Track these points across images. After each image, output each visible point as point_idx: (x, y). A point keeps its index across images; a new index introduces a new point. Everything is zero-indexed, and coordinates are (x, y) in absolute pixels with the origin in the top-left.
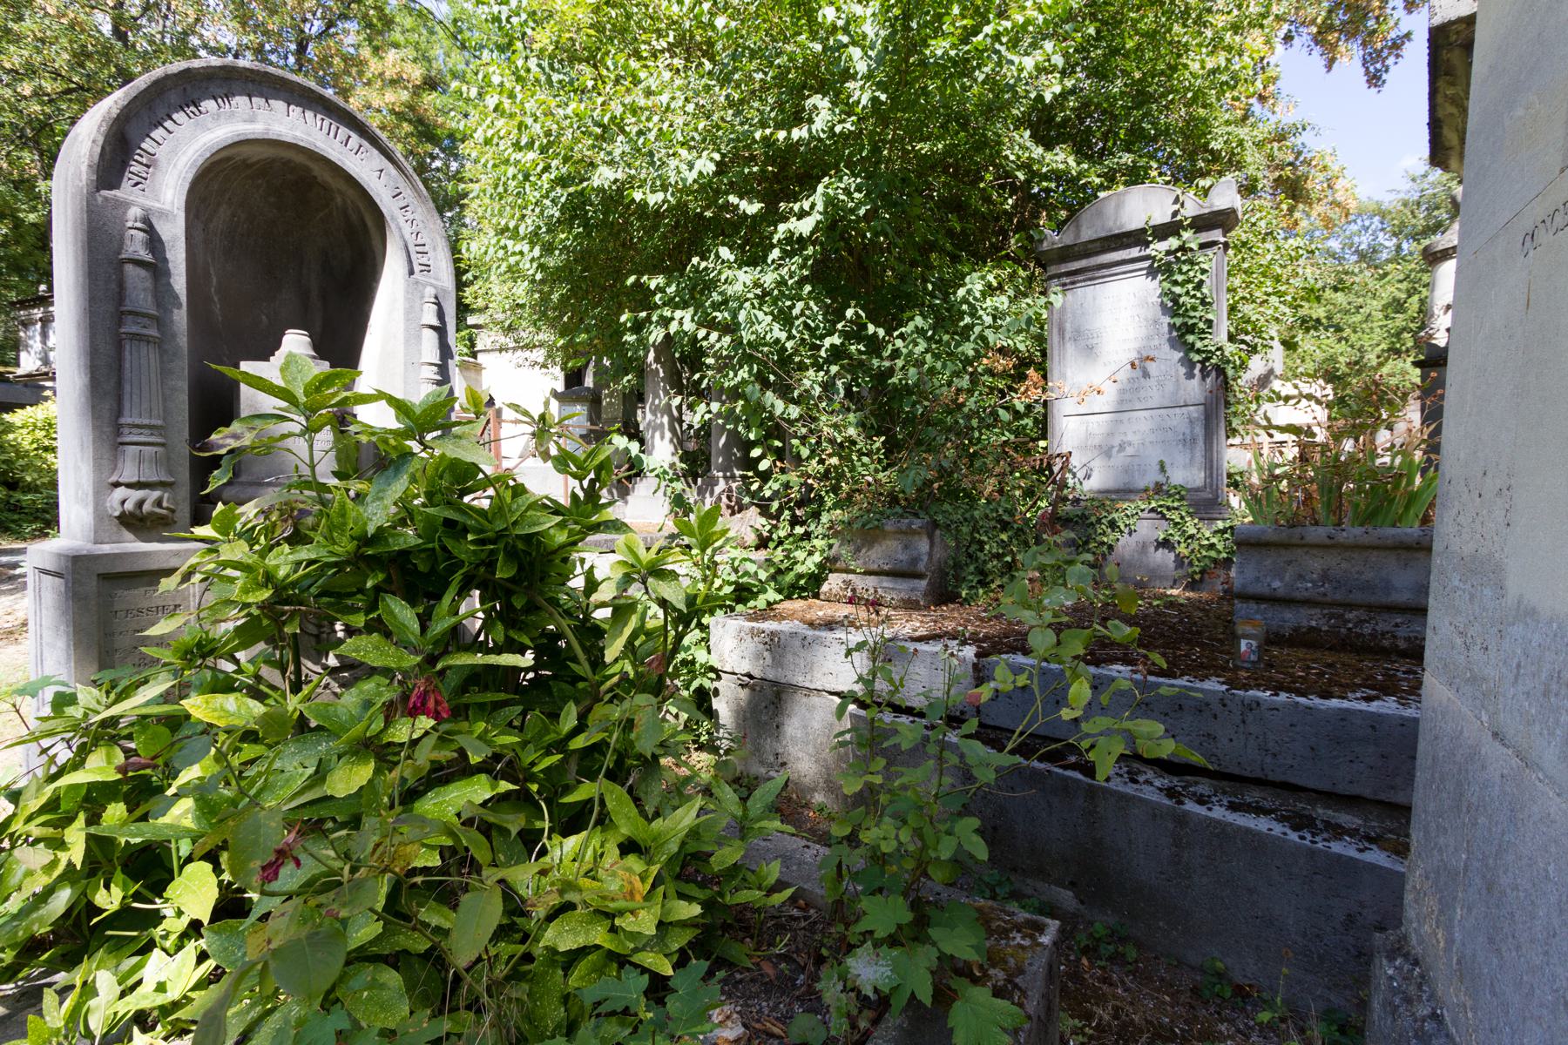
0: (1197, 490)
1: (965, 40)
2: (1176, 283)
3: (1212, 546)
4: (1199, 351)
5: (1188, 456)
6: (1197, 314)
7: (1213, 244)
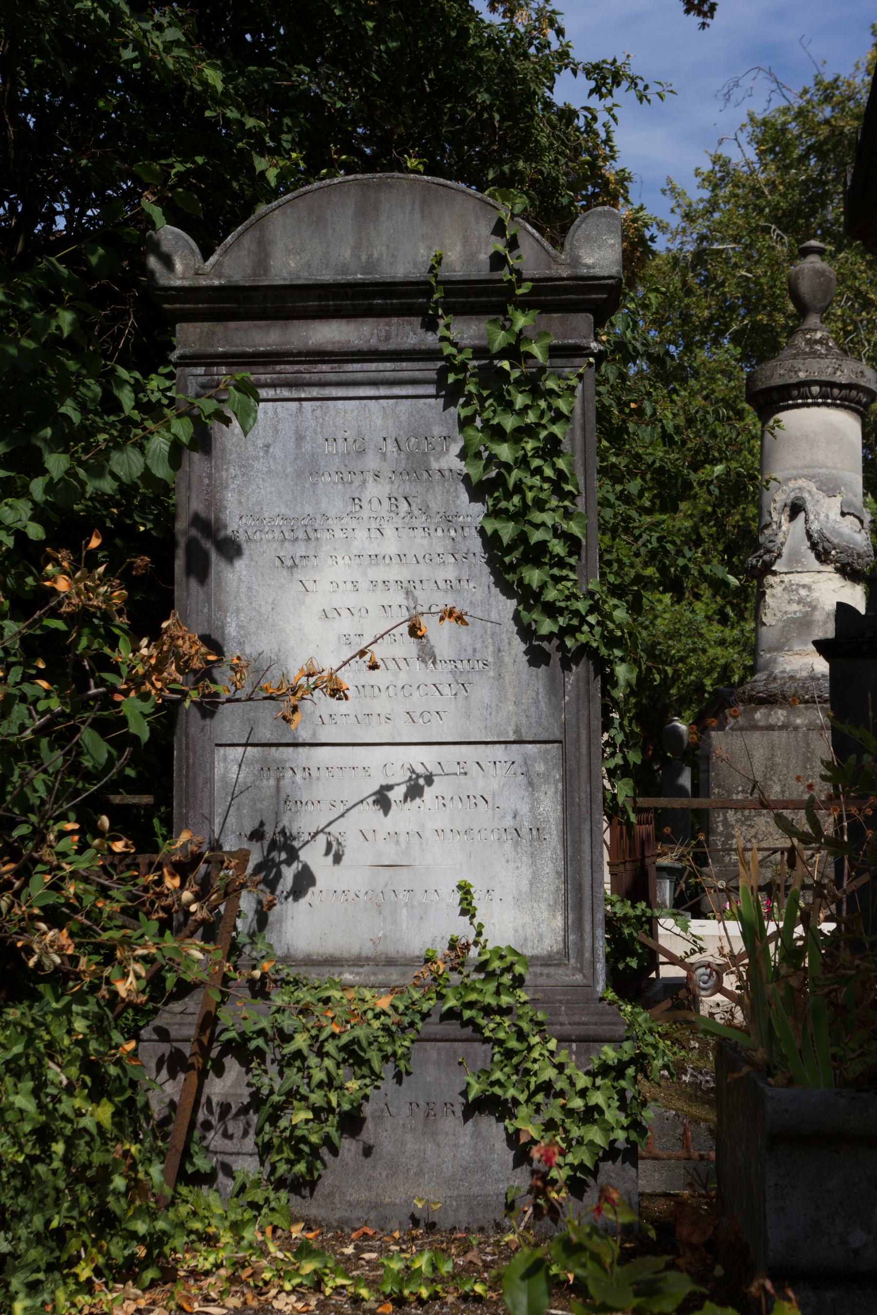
0: (547, 961)
1: (568, 598)
2: (497, 433)
3: (590, 1115)
4: (551, 610)
5: (526, 871)
6: (547, 518)
7: (578, 351)
